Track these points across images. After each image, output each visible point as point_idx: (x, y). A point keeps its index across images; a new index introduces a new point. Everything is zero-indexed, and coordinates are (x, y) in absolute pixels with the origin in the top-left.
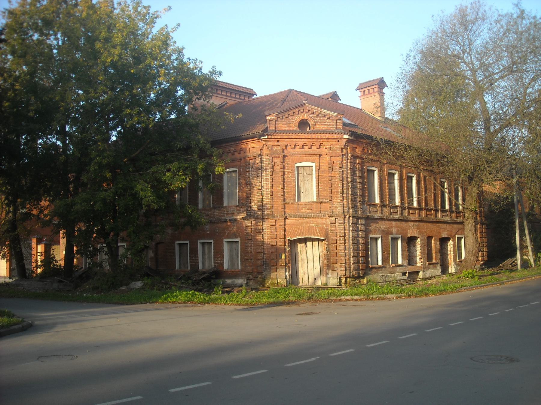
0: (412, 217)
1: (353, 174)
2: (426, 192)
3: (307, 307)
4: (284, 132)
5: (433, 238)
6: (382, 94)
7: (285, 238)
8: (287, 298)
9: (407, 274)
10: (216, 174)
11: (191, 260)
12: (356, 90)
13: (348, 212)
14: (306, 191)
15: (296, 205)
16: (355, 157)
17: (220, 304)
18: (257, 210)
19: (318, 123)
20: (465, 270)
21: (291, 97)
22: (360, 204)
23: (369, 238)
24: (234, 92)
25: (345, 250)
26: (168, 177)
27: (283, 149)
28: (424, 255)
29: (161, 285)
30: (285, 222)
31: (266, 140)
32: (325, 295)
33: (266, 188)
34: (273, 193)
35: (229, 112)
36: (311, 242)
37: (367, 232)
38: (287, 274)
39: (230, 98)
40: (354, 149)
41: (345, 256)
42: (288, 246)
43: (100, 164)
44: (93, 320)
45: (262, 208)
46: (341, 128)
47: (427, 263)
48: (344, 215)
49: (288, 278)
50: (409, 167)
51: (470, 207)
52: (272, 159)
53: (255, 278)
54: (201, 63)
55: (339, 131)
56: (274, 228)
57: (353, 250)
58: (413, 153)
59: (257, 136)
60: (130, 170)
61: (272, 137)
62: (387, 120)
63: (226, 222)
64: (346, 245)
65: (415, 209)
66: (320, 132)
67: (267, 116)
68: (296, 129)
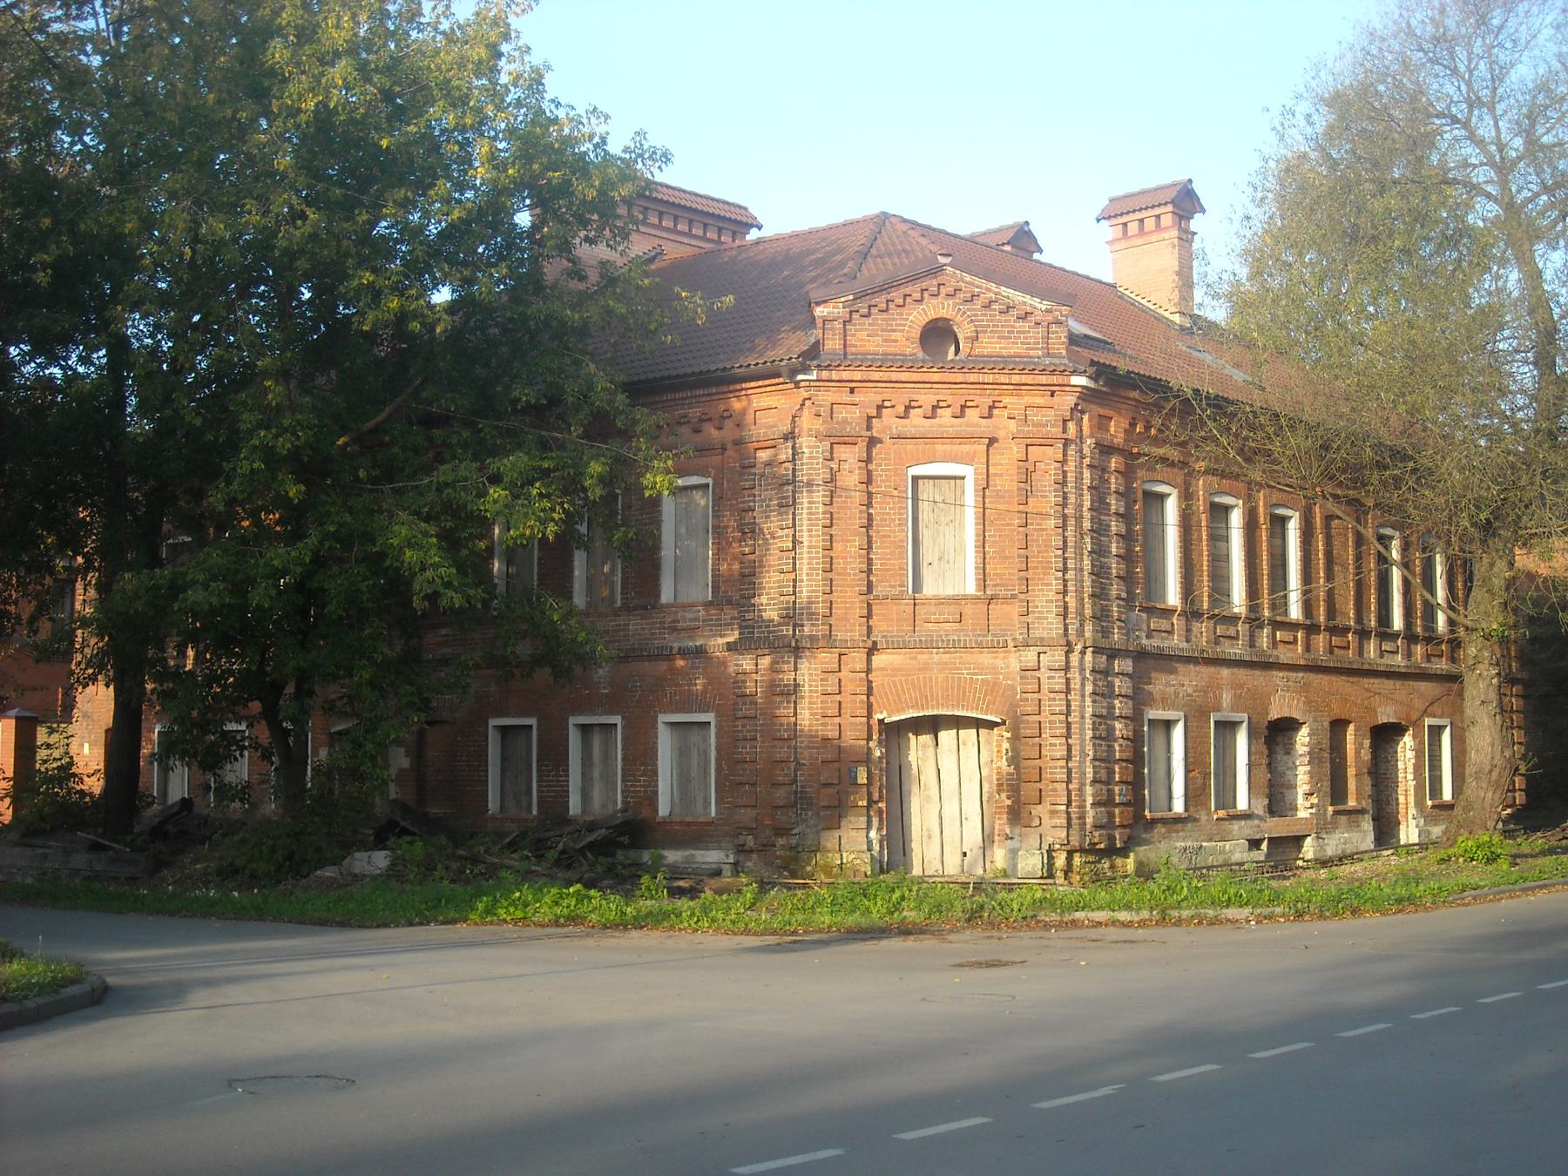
0: (1284, 654)
1: (1099, 506)
2: (1330, 577)
3: (969, 942)
4: (872, 360)
5: (1351, 727)
6: (1186, 237)
7: (869, 716)
8: (895, 915)
9: (1264, 846)
10: (647, 495)
11: (543, 781)
12: (1098, 220)
13: (1081, 633)
14: (940, 559)
15: (906, 604)
16: (1105, 449)
17: (680, 929)
18: (776, 618)
19: (986, 332)
20: (1466, 834)
21: (887, 240)
22: (1119, 606)
23: (1146, 722)
24: (686, 215)
25: (1069, 758)
26: (495, 502)
27: (869, 418)
28: (1320, 780)
29: (454, 866)
30: (869, 661)
31: (812, 384)
32: (1022, 905)
33: (810, 547)
34: (831, 565)
35: (692, 289)
36: (955, 731)
37: (1139, 699)
38: (873, 834)
39: (671, 236)
40: (1102, 423)
41: (1069, 781)
42: (880, 742)
43: (269, 454)
44: (298, 973)
45: (794, 613)
46: (1064, 352)
47: (1330, 809)
48: (1069, 644)
49: (878, 849)
50: (1287, 485)
51: (1484, 625)
52: (832, 448)
53: (765, 848)
54: (602, 119)
55: (1056, 361)
56: (833, 679)
57: (1095, 759)
58: (1297, 441)
59: (784, 371)
60: (362, 473)
61: (834, 375)
62: (1199, 327)
63: (670, 657)
64: (1070, 741)
65: (1294, 626)
66: (994, 362)
67: (818, 304)
68: (912, 348)
